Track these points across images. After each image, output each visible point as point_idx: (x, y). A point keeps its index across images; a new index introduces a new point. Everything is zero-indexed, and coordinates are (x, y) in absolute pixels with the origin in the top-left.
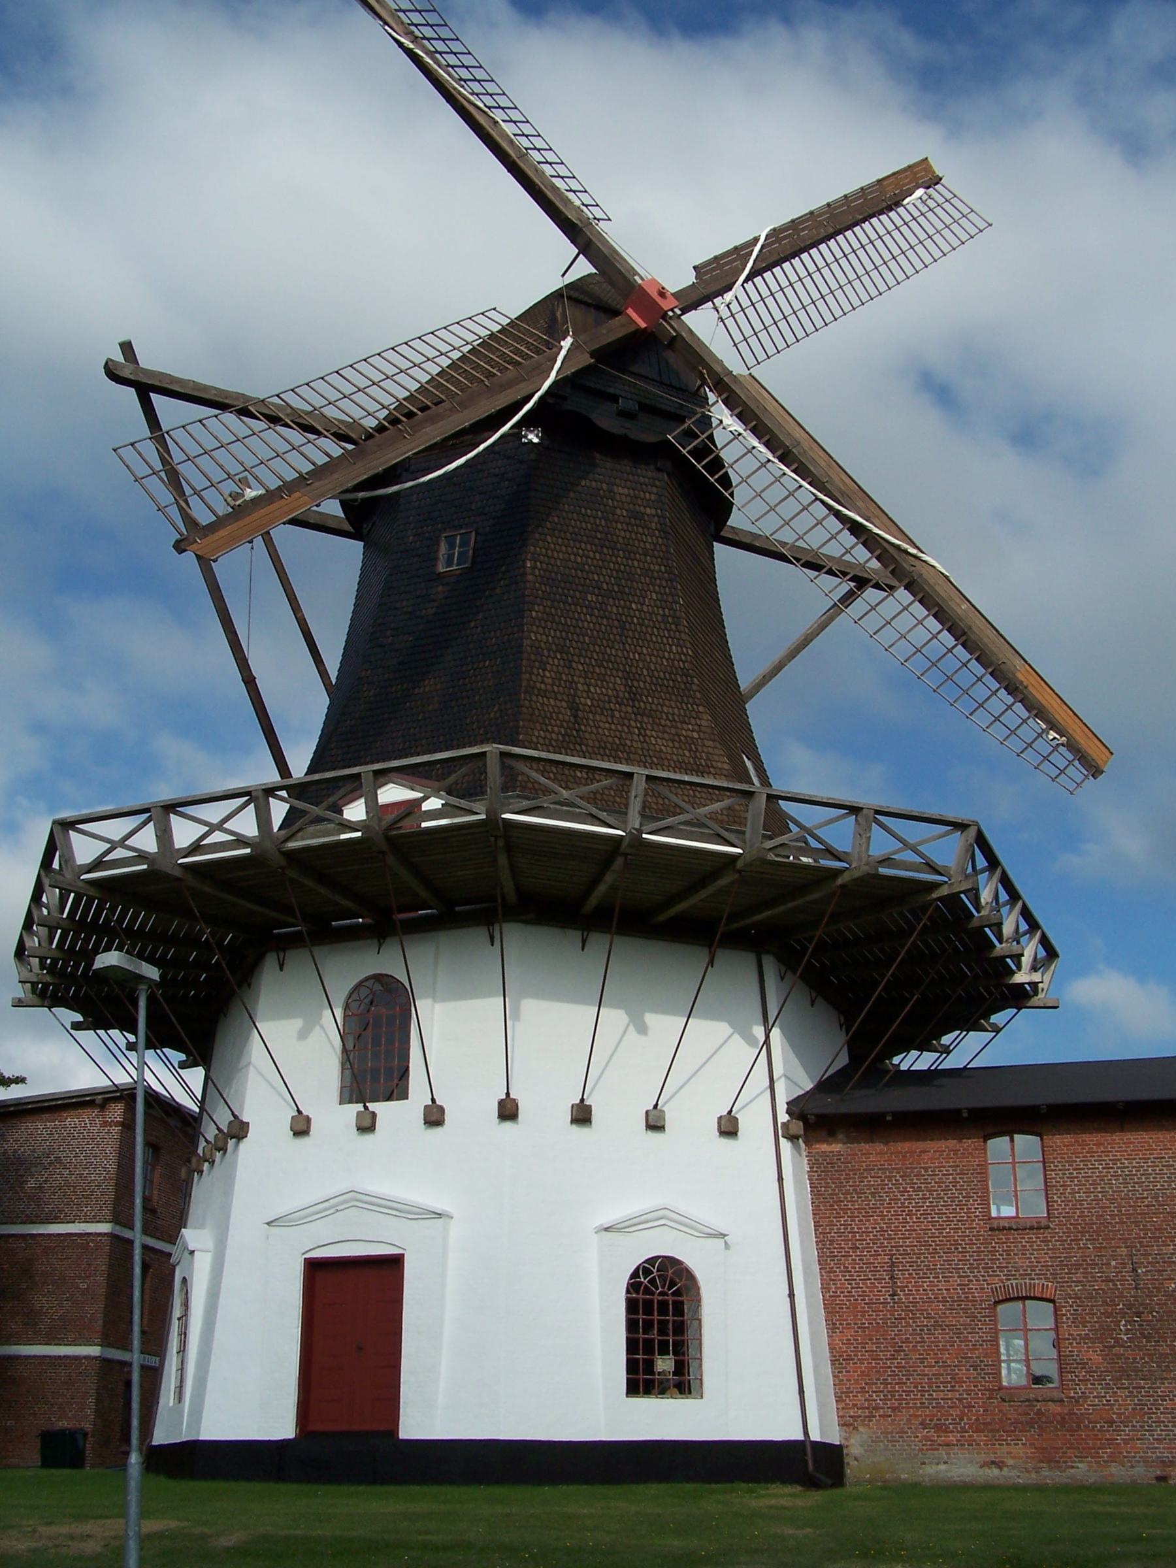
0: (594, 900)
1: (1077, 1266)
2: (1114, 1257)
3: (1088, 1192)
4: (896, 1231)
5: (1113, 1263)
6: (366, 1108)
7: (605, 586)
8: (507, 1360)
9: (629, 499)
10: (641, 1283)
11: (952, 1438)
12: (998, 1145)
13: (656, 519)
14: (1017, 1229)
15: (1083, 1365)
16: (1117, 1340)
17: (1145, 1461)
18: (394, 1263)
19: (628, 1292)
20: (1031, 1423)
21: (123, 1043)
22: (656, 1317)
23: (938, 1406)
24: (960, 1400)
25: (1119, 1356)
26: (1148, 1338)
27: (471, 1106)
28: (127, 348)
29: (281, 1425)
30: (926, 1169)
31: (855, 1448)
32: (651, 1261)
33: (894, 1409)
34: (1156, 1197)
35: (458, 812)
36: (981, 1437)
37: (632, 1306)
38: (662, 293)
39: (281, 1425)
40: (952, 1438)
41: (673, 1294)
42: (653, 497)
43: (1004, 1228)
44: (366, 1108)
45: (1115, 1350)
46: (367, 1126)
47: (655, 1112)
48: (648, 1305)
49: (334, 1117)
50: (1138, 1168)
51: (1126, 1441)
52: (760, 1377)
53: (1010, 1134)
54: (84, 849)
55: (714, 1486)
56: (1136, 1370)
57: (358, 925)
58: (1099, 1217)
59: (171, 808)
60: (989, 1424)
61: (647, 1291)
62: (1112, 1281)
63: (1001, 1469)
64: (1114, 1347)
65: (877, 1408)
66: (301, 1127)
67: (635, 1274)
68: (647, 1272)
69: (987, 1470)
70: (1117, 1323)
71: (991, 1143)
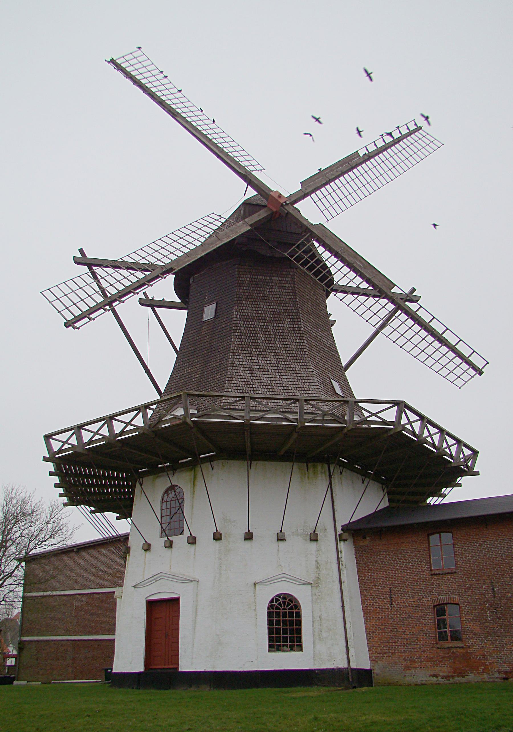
0: (286, 448)
1: (468, 588)
2: (484, 584)
3: (472, 556)
4: (392, 577)
5: (484, 587)
6: (168, 539)
7: (268, 319)
8: (223, 638)
9: (279, 282)
10: (275, 605)
11: (417, 665)
12: (434, 539)
13: (291, 288)
14: (442, 574)
15: (472, 631)
16: (486, 620)
17: (500, 672)
18: (176, 601)
19: (268, 608)
20: (449, 657)
21: (90, 510)
22: (281, 619)
23: (411, 652)
24: (420, 648)
25: (487, 627)
26: (499, 618)
27: (205, 536)
28: (81, 251)
29: (140, 668)
30: (403, 550)
31: (377, 670)
32: (279, 595)
33: (392, 653)
34: (502, 556)
35: (232, 418)
36: (429, 664)
37: (270, 614)
38: (280, 196)
39: (140, 668)
40: (417, 665)
41: (289, 609)
42: (289, 279)
43: (437, 574)
44: (168, 539)
45: (485, 624)
46: (170, 545)
47: (281, 534)
48: (278, 614)
49: (158, 542)
50: (494, 545)
51: (490, 664)
52: (332, 642)
53: (439, 533)
54: (56, 446)
55: (283, 689)
56: (494, 632)
57: (189, 461)
58: (477, 566)
59: (80, 427)
60: (432, 658)
61: (277, 608)
62: (484, 594)
63: (437, 677)
64: (484, 623)
65: (385, 653)
66: (147, 547)
67: (272, 601)
68: (277, 600)
69: (431, 678)
70: (486, 613)
71: (431, 537)
